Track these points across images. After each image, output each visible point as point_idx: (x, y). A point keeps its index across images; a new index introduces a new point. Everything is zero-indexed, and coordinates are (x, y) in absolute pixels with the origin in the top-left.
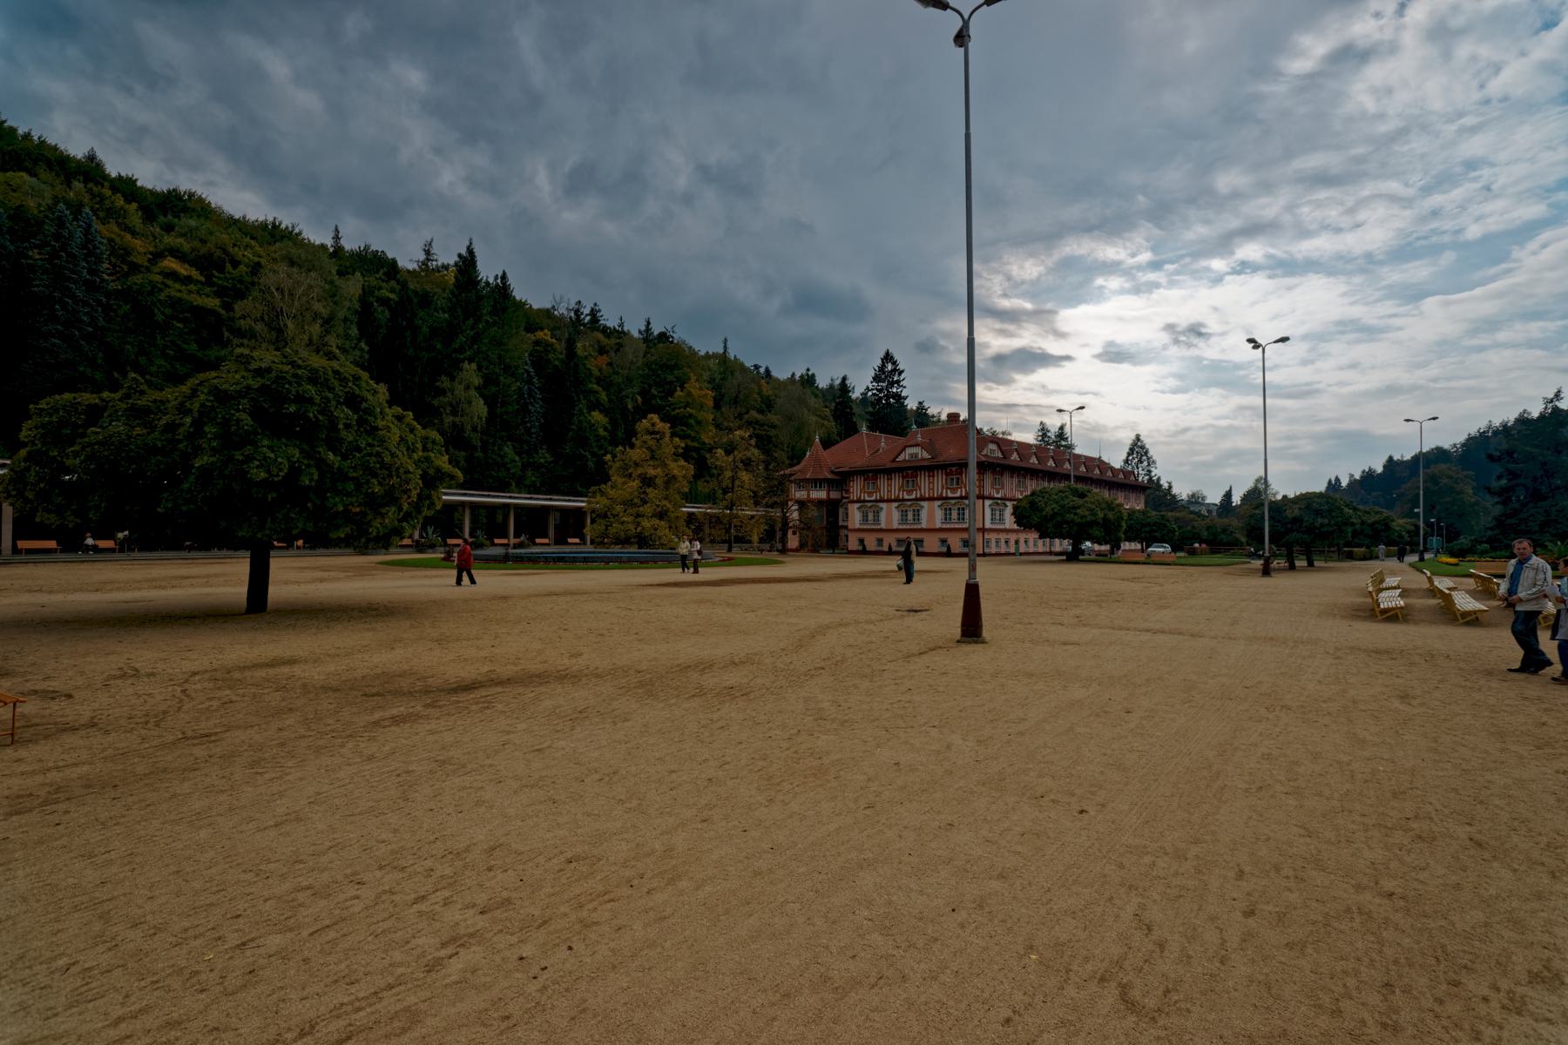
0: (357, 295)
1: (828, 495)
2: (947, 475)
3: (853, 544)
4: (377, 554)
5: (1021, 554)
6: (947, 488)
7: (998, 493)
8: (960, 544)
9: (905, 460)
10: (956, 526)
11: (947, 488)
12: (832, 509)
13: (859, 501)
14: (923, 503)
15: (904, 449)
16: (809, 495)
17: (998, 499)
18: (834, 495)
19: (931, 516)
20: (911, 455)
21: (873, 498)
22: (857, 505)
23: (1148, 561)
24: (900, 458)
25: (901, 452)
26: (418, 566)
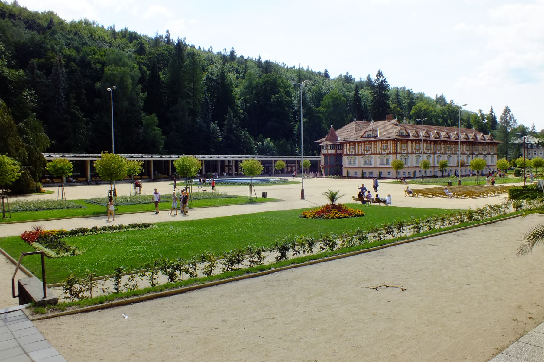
0: (30, 32)
1: (336, 152)
2: (382, 144)
3: (345, 174)
4: (37, 202)
5: (417, 178)
6: (382, 150)
7: (428, 151)
8: (387, 174)
10: (385, 166)
11: (382, 150)
12: (339, 157)
13: (347, 155)
14: (390, 155)
16: (327, 152)
17: (468, 154)
18: (339, 151)
19: (376, 162)
21: (353, 154)
22: (347, 157)
23: (389, 176)
26: (144, 301)
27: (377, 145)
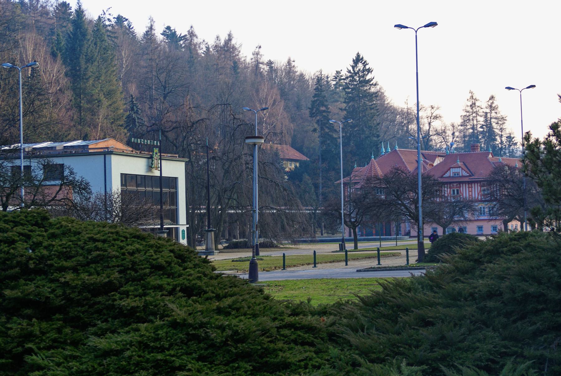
2: (450, 188)
9: (450, 177)
15: (449, 169)
20: (454, 173)
24: (447, 175)
25: (447, 171)
27: (473, 188)
